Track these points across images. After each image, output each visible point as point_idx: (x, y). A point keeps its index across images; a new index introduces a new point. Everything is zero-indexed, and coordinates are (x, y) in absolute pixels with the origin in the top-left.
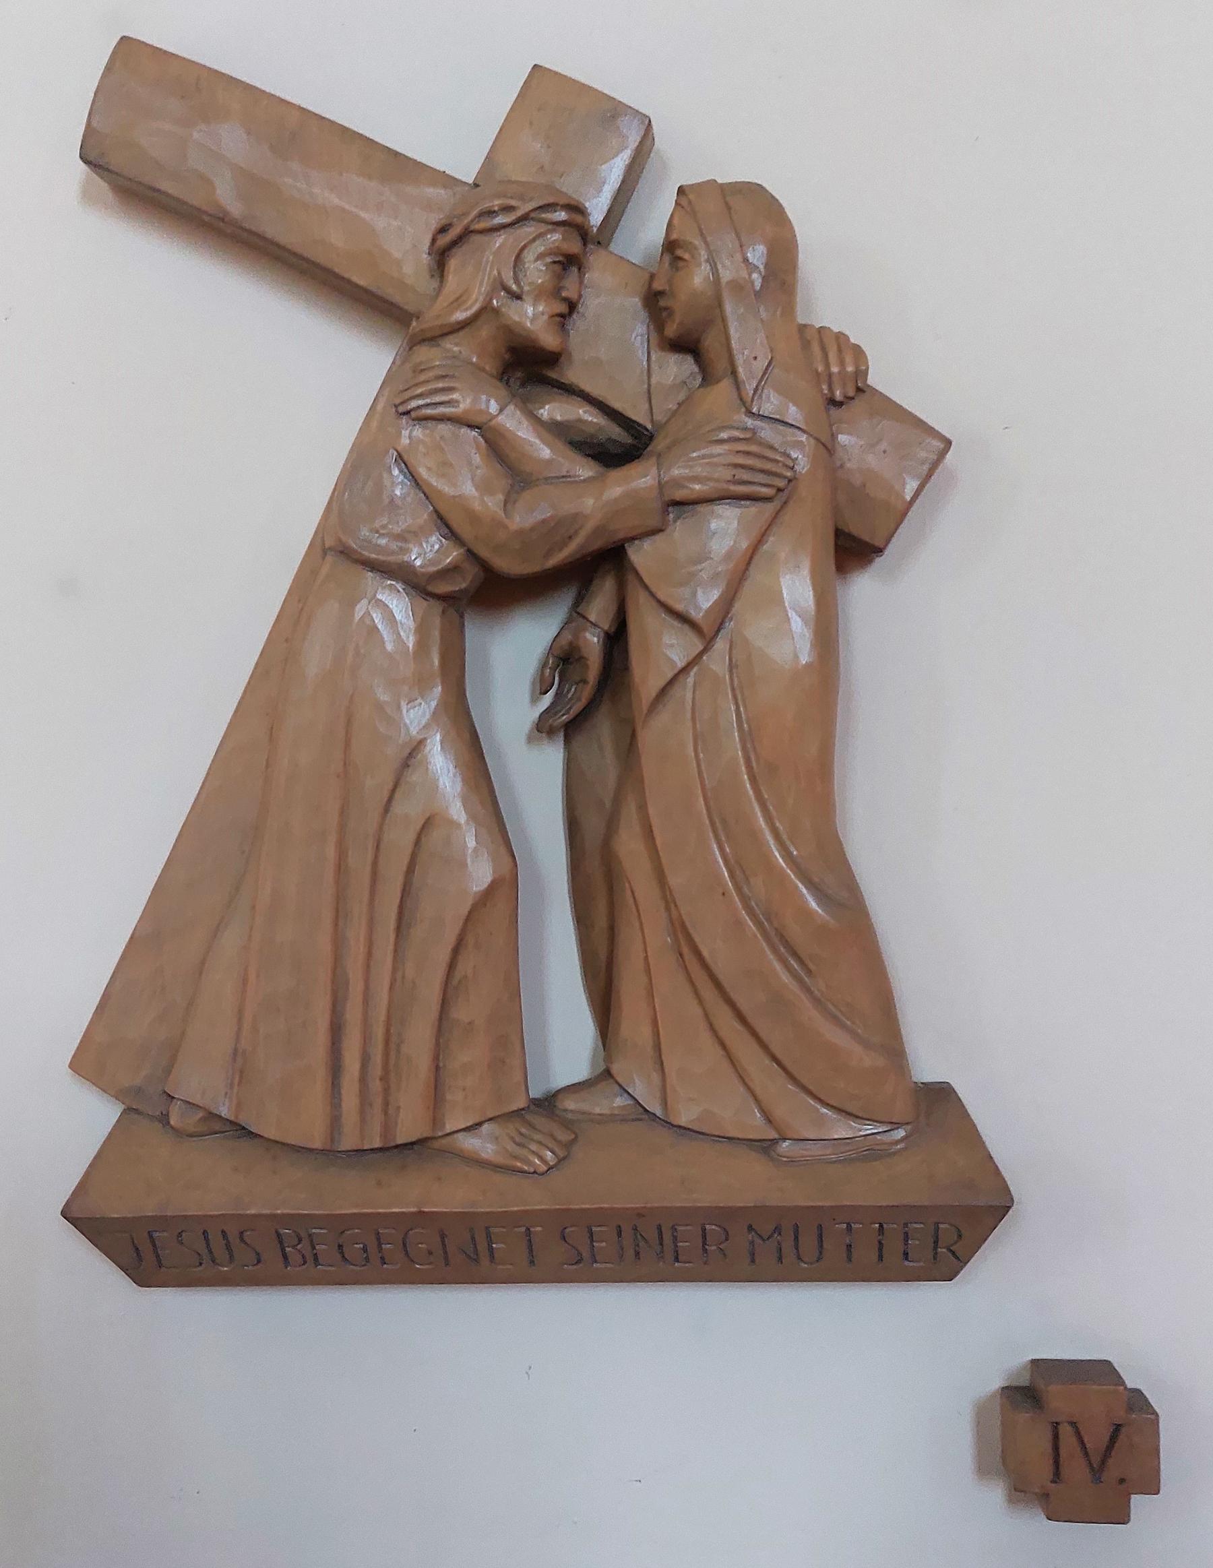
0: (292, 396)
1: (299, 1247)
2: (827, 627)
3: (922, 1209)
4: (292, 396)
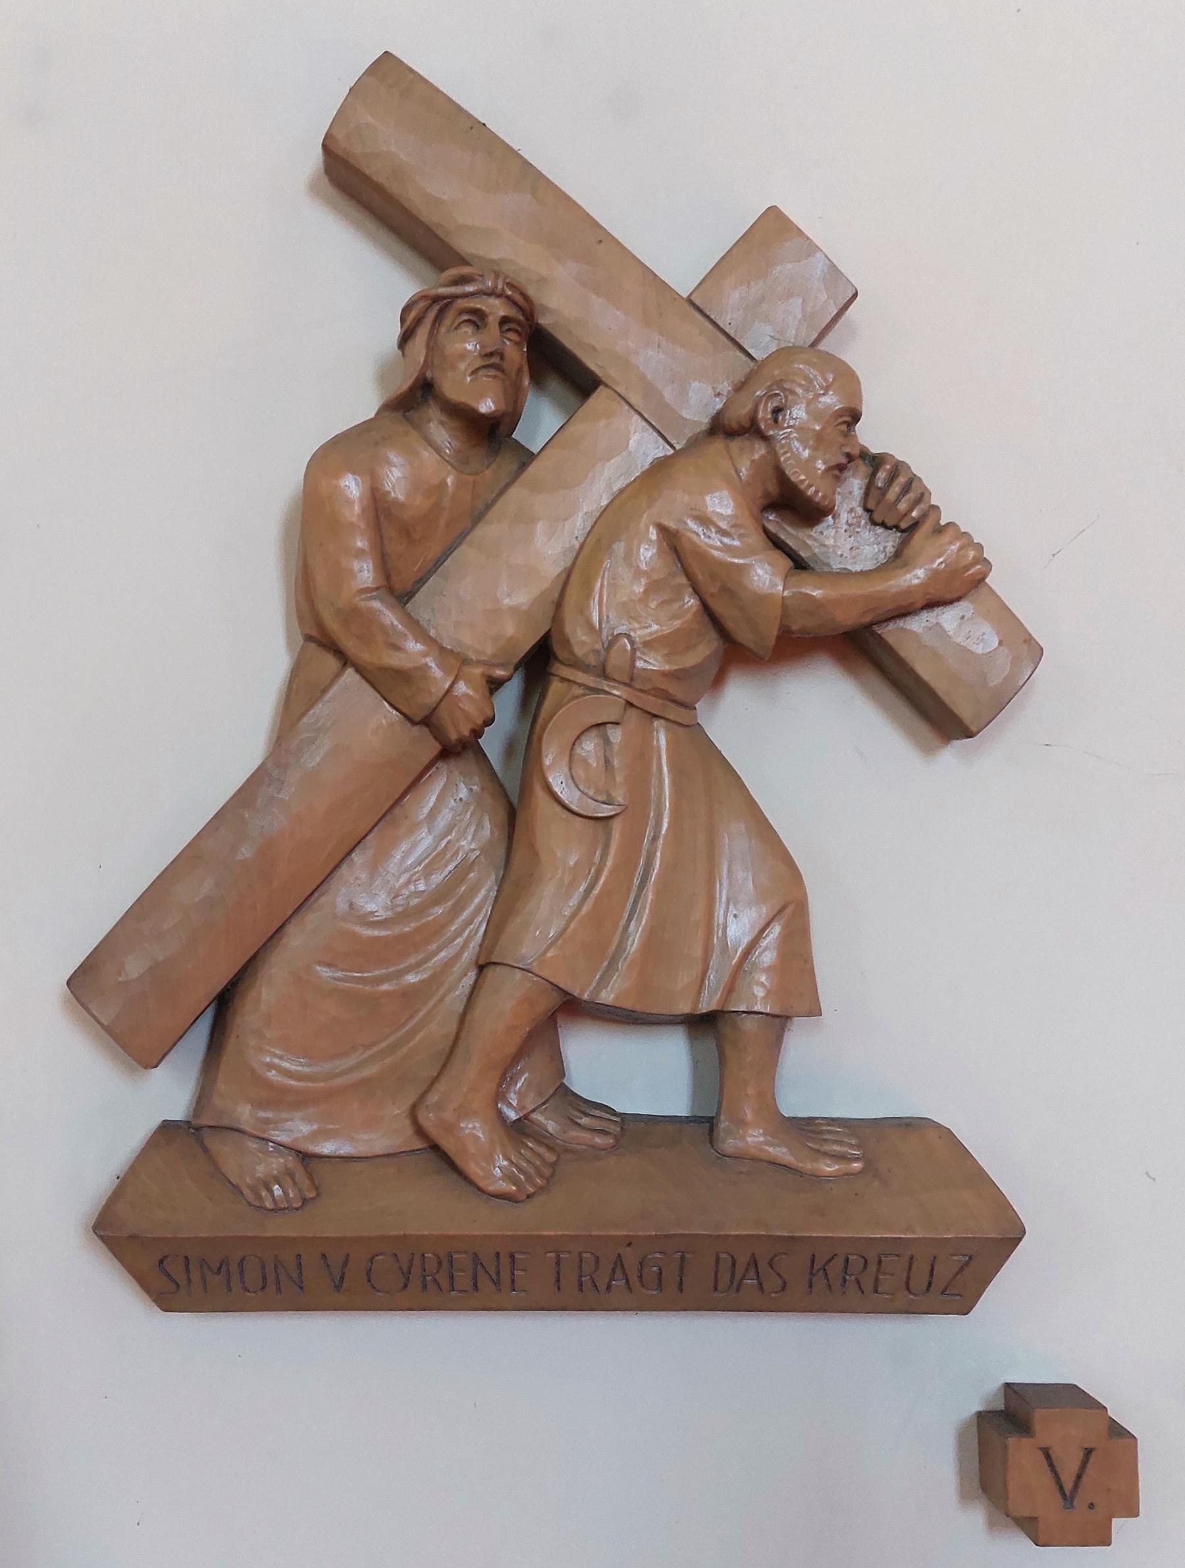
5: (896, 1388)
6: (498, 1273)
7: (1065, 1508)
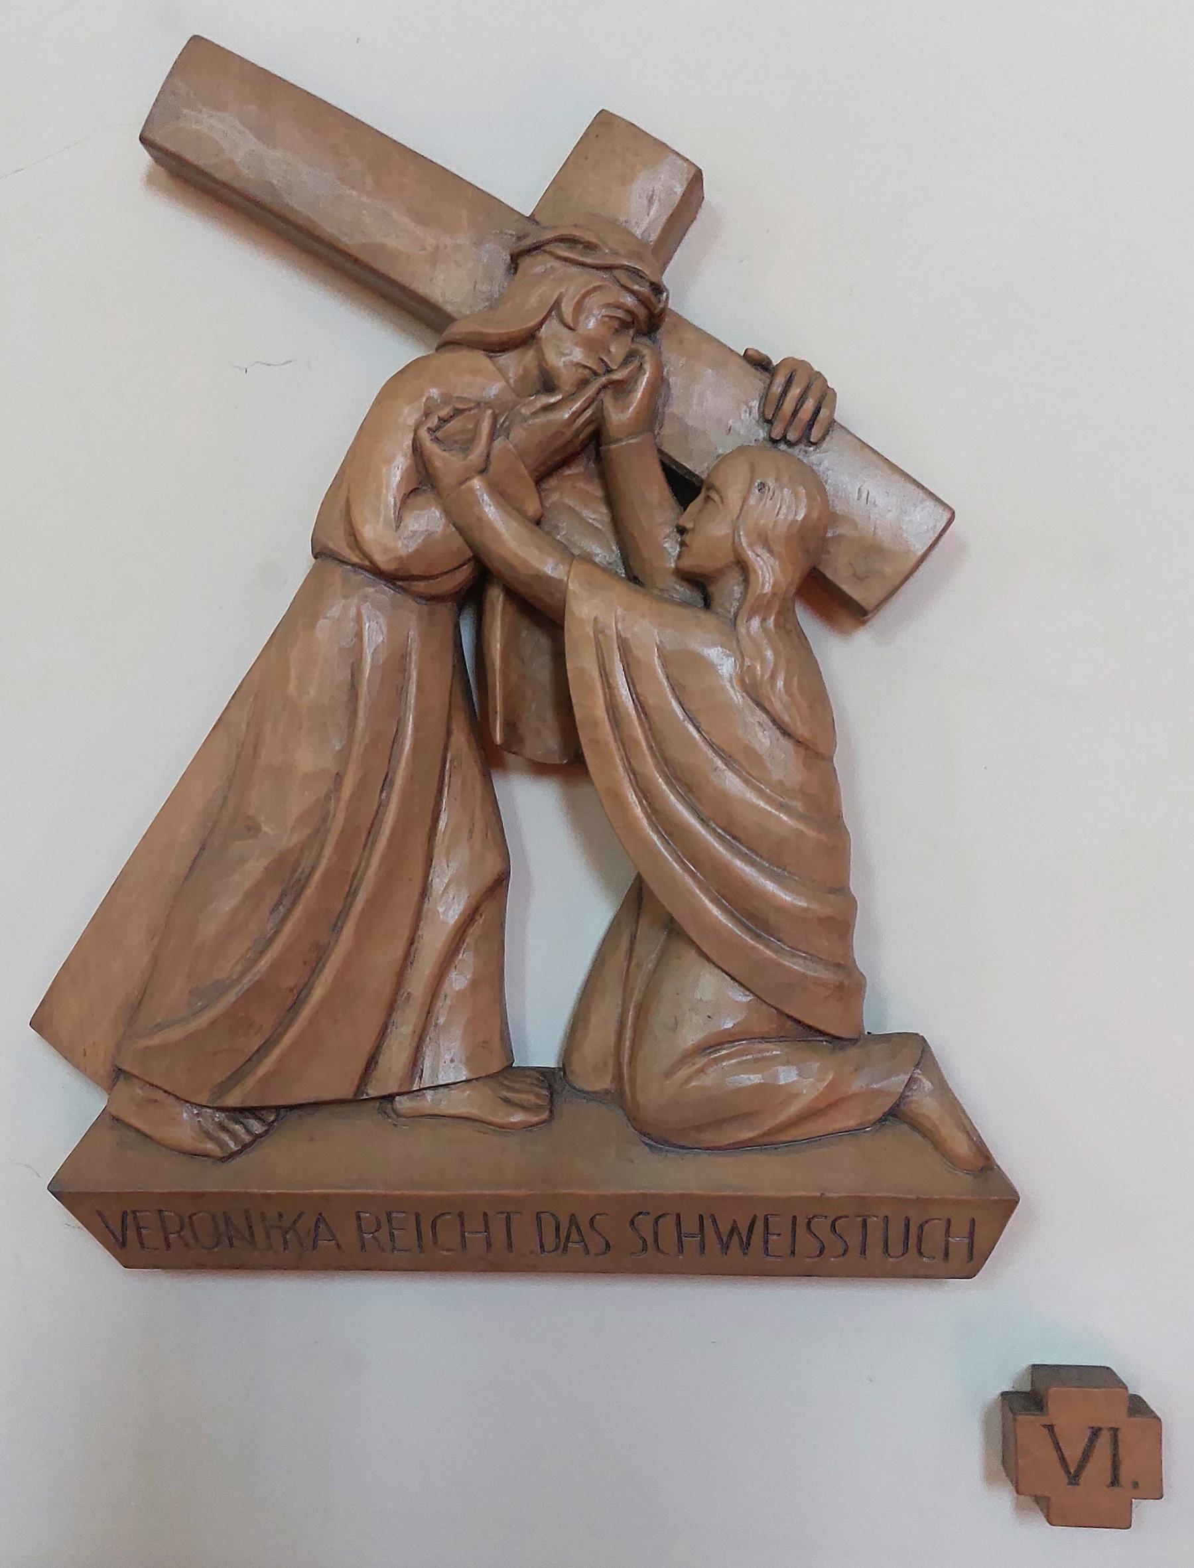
0: (335, 366)
1: (376, 1234)
2: (814, 741)
3: (933, 1211)
4: (335, 366)
5: (902, 1367)
6: (749, 1238)
7: (1070, 1483)
